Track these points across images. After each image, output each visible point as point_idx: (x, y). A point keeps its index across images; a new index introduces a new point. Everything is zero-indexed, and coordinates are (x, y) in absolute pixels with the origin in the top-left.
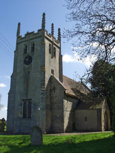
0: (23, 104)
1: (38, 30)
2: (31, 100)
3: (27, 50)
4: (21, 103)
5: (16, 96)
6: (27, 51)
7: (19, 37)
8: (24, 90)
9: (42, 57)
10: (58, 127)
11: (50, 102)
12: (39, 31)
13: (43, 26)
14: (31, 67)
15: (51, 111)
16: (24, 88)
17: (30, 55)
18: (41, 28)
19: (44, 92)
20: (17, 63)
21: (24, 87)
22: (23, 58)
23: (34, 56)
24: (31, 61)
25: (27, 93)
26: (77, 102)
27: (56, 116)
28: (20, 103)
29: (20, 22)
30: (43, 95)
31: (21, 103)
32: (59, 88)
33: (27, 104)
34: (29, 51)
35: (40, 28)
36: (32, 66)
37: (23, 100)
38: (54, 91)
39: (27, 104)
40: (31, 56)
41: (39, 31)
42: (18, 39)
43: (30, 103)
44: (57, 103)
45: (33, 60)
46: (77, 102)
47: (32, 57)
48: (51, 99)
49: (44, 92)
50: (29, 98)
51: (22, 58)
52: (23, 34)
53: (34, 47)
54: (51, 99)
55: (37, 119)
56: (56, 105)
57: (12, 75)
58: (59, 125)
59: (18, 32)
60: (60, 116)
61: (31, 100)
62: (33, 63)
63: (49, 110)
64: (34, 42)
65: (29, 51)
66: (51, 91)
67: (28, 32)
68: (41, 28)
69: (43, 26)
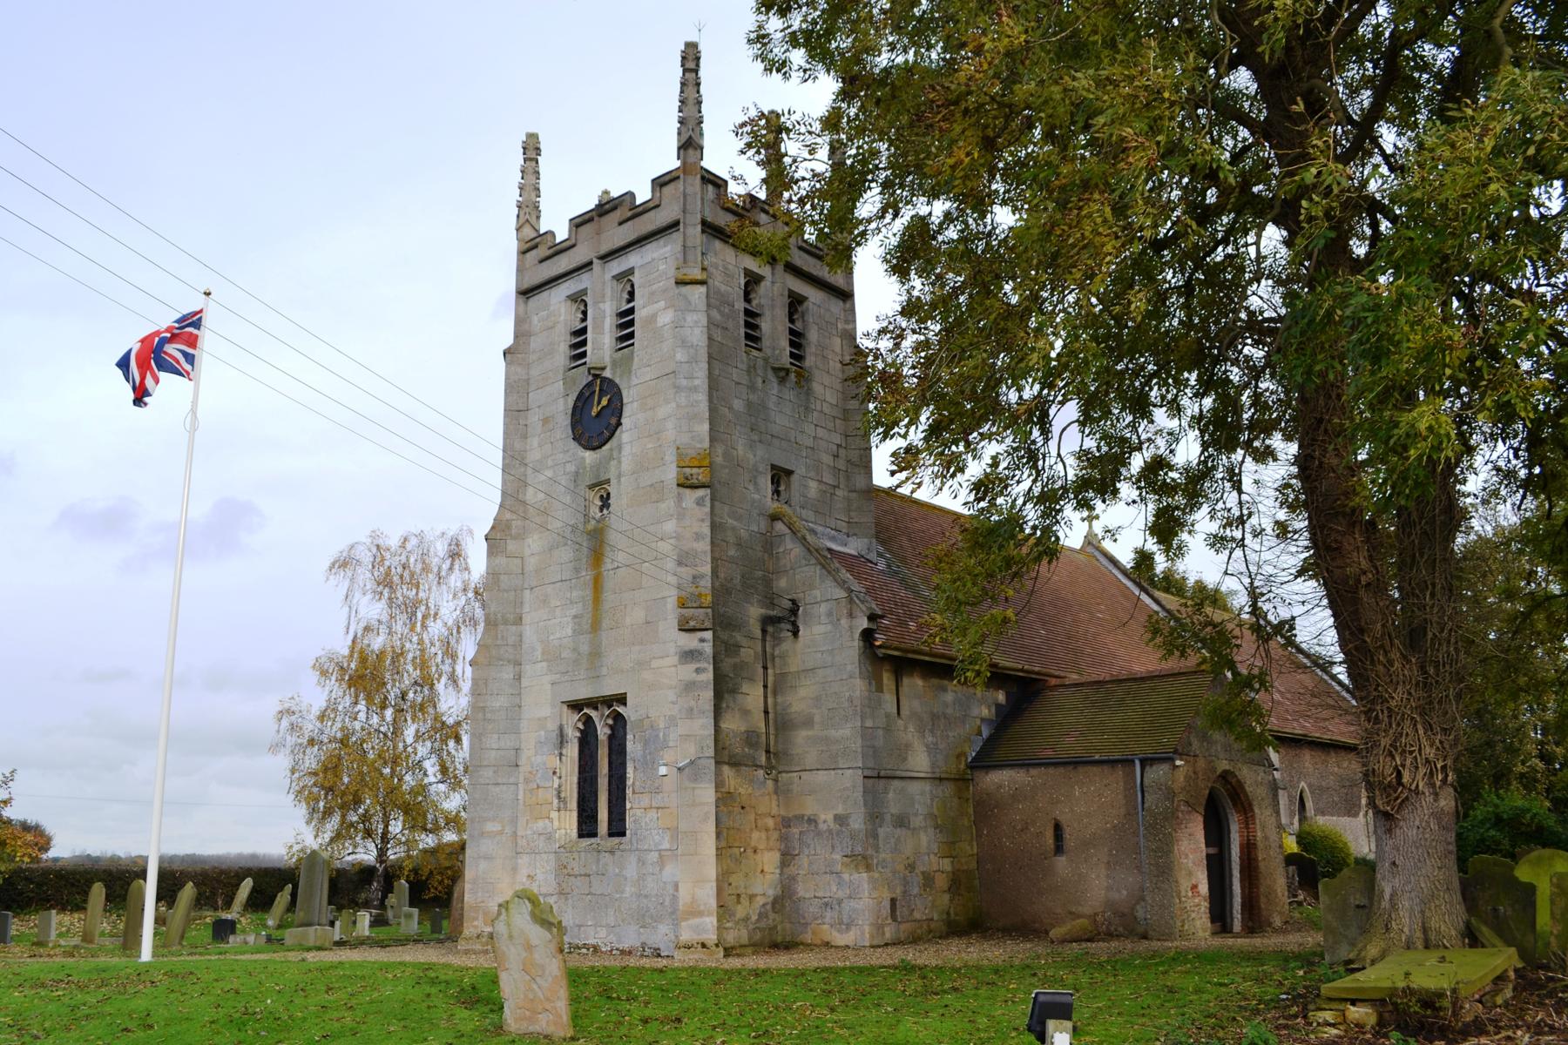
0: (573, 735)
1: (653, 181)
2: (622, 700)
3: (589, 335)
4: (561, 729)
5: (525, 682)
6: (589, 348)
7: (534, 244)
8: (574, 631)
9: (684, 382)
10: (826, 904)
11: (766, 712)
12: (663, 185)
13: (690, 144)
14: (620, 462)
15: (776, 781)
16: (575, 617)
17: (607, 374)
18: (678, 164)
19: (702, 640)
20: (525, 437)
21: (574, 612)
22: (561, 401)
23: (635, 381)
24: (613, 421)
25: (596, 655)
26: (998, 706)
27: (812, 821)
28: (552, 726)
29: (532, 130)
30: (694, 666)
31: (561, 729)
32: (823, 608)
33: (603, 732)
34: (602, 343)
35: (669, 161)
36: (626, 450)
37: (576, 706)
38: (796, 633)
39: (603, 732)
40: (617, 381)
41: (660, 183)
42: (528, 255)
43: (619, 722)
44: (817, 719)
45: (627, 411)
46: (998, 706)
47: (623, 386)
48: (775, 694)
49: (702, 640)
50: (609, 689)
51: (556, 401)
52: (556, 221)
53: (631, 311)
54: (775, 694)
55: (1523, 680)
56: (810, 733)
57: (493, 528)
58: (834, 889)
59: (529, 209)
60: (837, 818)
61: (622, 700)
62: (625, 435)
63: (761, 772)
64: (631, 271)
65: (602, 343)
66: (770, 629)
67: (606, 192)
68: (671, 162)
69: (690, 144)
